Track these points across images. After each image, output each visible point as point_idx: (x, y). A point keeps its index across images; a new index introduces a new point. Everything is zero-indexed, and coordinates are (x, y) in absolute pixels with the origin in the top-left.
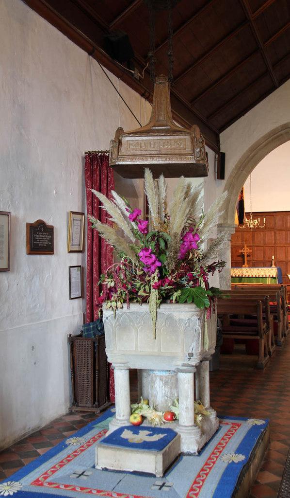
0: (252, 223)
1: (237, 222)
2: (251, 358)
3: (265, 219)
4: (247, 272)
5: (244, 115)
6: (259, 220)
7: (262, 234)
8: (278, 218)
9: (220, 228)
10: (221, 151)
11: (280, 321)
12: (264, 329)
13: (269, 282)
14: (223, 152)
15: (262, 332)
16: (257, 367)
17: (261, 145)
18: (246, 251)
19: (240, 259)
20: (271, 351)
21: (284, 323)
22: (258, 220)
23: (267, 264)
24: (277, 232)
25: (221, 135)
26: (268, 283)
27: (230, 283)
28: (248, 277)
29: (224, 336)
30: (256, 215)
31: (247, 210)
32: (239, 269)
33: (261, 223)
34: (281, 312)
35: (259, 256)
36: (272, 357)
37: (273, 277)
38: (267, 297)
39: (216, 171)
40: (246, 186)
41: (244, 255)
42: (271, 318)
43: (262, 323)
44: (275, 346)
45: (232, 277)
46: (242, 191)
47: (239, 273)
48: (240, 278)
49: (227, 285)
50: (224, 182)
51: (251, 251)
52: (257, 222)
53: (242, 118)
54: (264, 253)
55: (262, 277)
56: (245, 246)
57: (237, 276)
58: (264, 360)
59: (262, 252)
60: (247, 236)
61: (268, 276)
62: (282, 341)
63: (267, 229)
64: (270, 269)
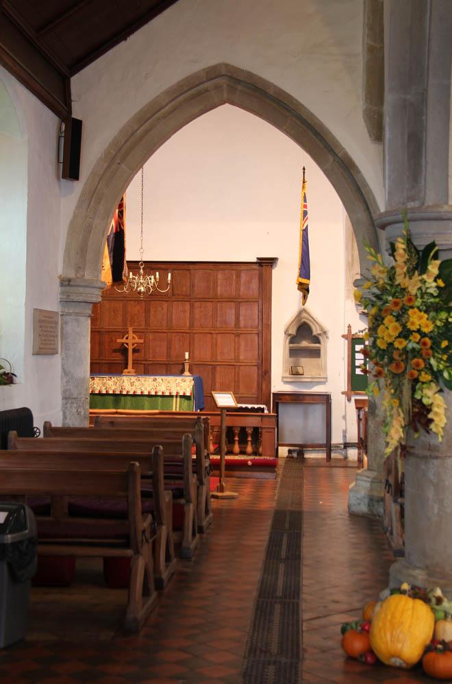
0: (143, 283)
1: (106, 275)
2: (113, 596)
3: (170, 275)
4: (132, 384)
5: (126, 39)
6: (157, 276)
7: (164, 306)
8: (199, 274)
9: (67, 289)
10: (73, 116)
11: (189, 501)
12: (144, 532)
13: (176, 406)
14: (79, 118)
15: (139, 538)
16: (121, 624)
17: (163, 111)
18: (131, 340)
19: (118, 357)
20: (165, 575)
21: (198, 504)
22: (155, 278)
23: (173, 368)
24: (197, 304)
25: (75, 80)
26: (174, 410)
27: (87, 410)
28: (134, 395)
29: (42, 549)
30: (151, 266)
31: (131, 255)
32: (114, 379)
33: (162, 283)
34: (193, 479)
35: (159, 351)
36: (166, 590)
37: (184, 397)
38: (157, 449)
39: (61, 160)
40: (131, 196)
41: (126, 350)
42: (166, 497)
43: (139, 516)
44: (174, 561)
45: (92, 394)
46: (121, 206)
47: (113, 388)
48: (117, 398)
49: (79, 413)
50: (78, 187)
51: (142, 341)
52: (153, 281)
53: (122, 46)
54: (169, 348)
55: (163, 396)
56: (130, 330)
57: (111, 392)
58: (140, 608)
59: (165, 343)
60: (135, 309)
61: (174, 394)
62: (192, 546)
63: (174, 296)
64: (179, 379)
